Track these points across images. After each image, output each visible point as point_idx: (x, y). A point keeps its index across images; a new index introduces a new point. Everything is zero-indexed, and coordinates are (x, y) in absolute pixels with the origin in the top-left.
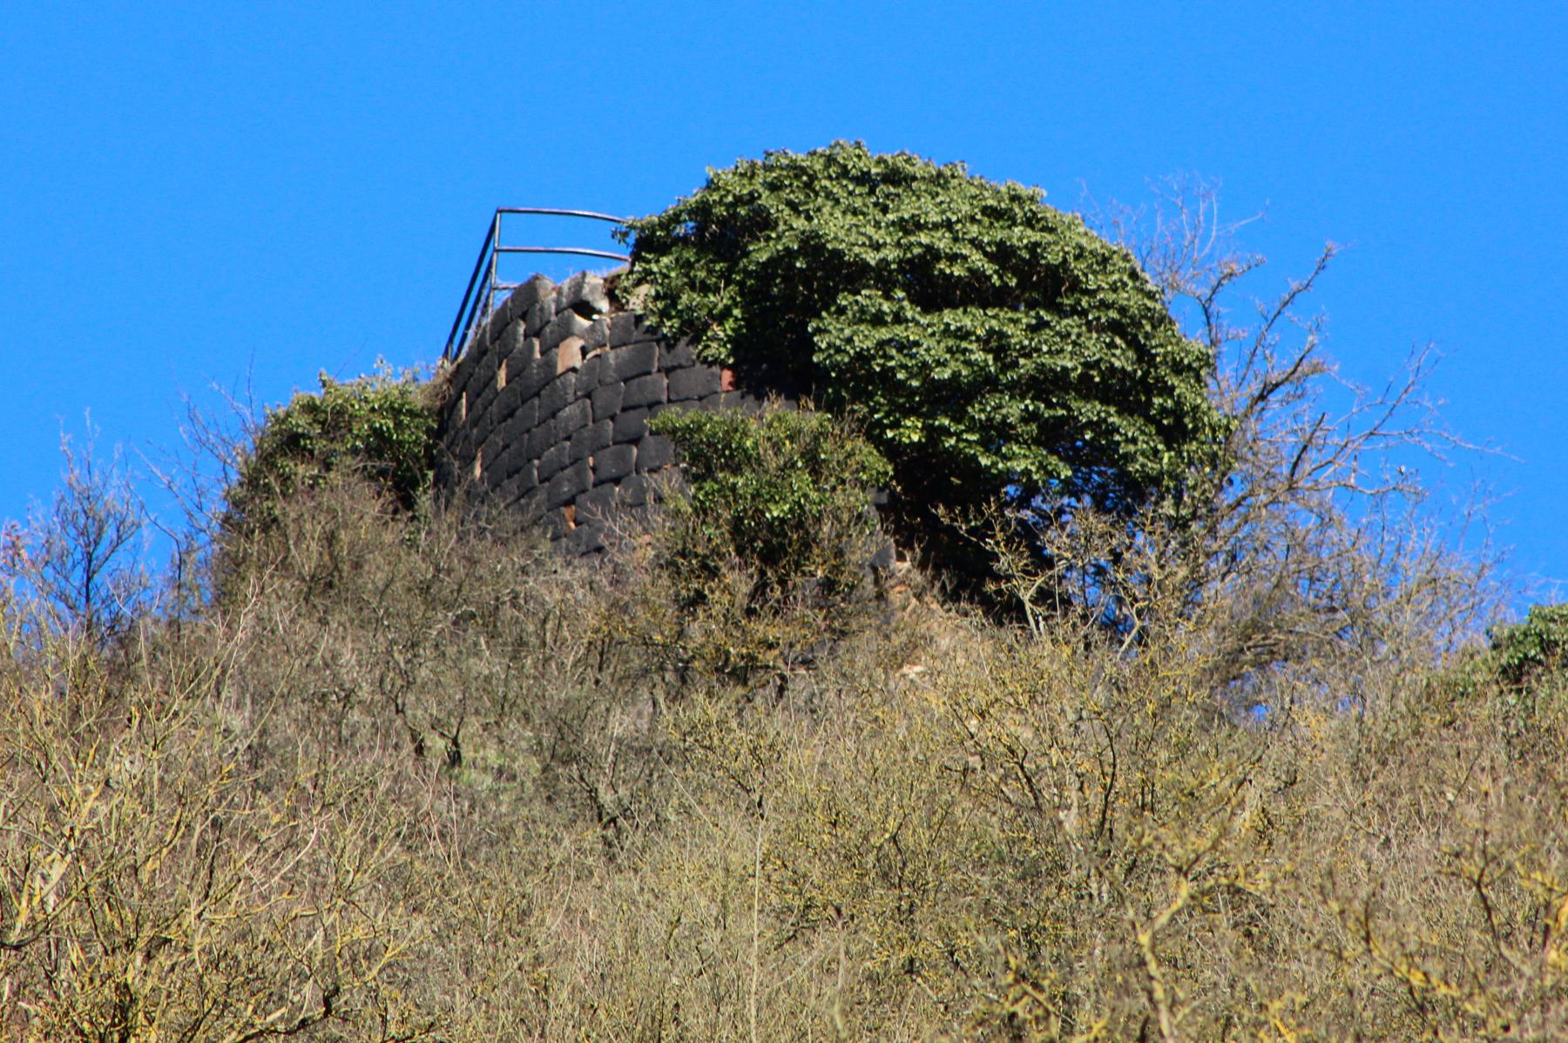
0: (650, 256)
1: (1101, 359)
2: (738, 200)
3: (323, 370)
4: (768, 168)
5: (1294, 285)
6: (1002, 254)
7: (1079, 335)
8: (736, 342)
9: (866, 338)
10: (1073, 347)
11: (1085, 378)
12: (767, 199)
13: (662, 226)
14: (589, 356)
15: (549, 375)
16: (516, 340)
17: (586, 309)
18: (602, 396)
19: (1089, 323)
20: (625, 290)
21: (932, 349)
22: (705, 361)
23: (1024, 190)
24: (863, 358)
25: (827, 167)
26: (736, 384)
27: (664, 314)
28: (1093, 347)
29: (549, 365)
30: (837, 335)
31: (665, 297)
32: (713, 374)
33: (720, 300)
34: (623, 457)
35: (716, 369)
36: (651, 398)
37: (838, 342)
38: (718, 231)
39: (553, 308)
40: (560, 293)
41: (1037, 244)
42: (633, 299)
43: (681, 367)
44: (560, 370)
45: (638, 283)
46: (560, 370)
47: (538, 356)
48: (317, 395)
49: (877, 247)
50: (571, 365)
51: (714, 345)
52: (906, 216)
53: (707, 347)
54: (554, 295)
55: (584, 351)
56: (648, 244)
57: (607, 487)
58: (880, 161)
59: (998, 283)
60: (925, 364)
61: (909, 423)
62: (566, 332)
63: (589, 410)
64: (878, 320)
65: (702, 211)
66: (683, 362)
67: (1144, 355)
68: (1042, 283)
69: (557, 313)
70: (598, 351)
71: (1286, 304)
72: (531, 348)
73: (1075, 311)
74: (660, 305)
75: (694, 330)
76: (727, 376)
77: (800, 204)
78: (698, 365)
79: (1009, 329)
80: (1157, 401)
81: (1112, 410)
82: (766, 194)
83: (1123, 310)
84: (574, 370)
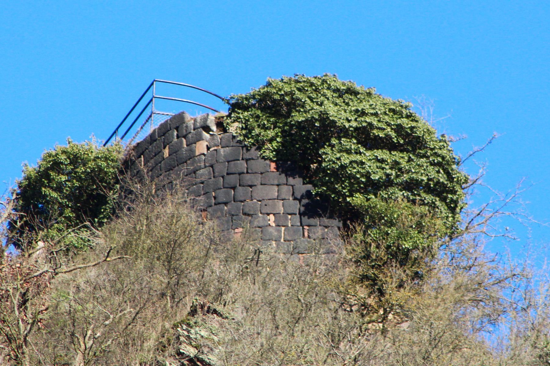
0: (240, 111)
1: (434, 178)
2: (286, 94)
3: (69, 137)
4: (297, 82)
5: (476, 148)
6: (399, 129)
7: (427, 166)
8: (277, 151)
9: (346, 159)
10: (425, 171)
11: (428, 184)
12: (298, 94)
13: (246, 99)
14: (211, 150)
15: (192, 156)
16: (173, 138)
17: (207, 129)
18: (217, 168)
19: (430, 162)
20: (228, 124)
21: (371, 166)
22: (263, 158)
23: (404, 103)
24: (343, 167)
25: (322, 84)
26: (277, 168)
27: (245, 136)
28: (433, 173)
29: (192, 151)
30: (331, 155)
31: (246, 128)
32: (267, 164)
33: (271, 133)
34: (228, 194)
35: (268, 162)
36: (240, 171)
37: (334, 159)
38: (272, 105)
39: (192, 127)
40: (195, 120)
41: (414, 127)
42: (231, 128)
43: (253, 159)
44: (197, 154)
45: (234, 121)
46: (197, 154)
47: (185, 146)
48: (68, 148)
49: (349, 121)
50: (202, 152)
51: (267, 151)
52: (360, 109)
53: (264, 152)
54: (192, 121)
55: (208, 148)
56: (237, 106)
57: (222, 206)
58: (344, 84)
59: (396, 141)
60: (368, 172)
61: (357, 196)
62: (200, 138)
63: (212, 172)
64: (348, 152)
65: (266, 96)
66: (254, 158)
67: (450, 177)
68: (412, 142)
69: (194, 129)
70: (216, 148)
71: (471, 155)
72: (181, 142)
73: (424, 156)
74: (244, 132)
75: (259, 145)
76: (273, 165)
77: (314, 98)
78: (260, 159)
79: (401, 161)
80: (450, 196)
81: (438, 199)
82: (297, 92)
83: (443, 158)
84: (204, 154)
